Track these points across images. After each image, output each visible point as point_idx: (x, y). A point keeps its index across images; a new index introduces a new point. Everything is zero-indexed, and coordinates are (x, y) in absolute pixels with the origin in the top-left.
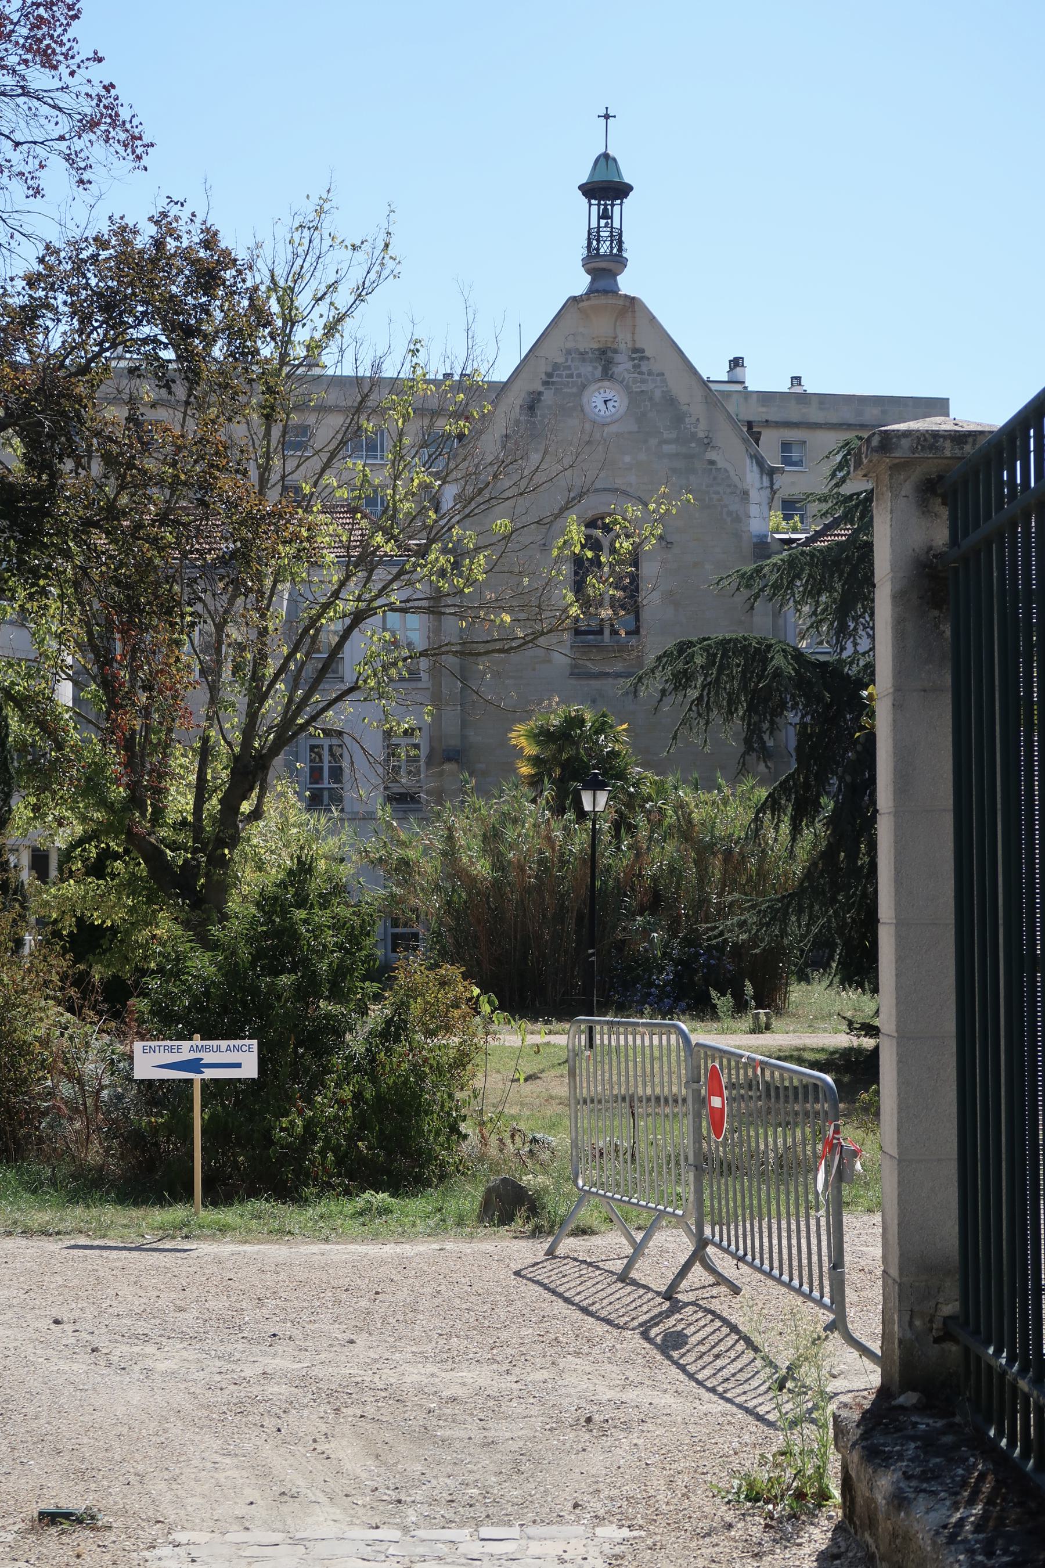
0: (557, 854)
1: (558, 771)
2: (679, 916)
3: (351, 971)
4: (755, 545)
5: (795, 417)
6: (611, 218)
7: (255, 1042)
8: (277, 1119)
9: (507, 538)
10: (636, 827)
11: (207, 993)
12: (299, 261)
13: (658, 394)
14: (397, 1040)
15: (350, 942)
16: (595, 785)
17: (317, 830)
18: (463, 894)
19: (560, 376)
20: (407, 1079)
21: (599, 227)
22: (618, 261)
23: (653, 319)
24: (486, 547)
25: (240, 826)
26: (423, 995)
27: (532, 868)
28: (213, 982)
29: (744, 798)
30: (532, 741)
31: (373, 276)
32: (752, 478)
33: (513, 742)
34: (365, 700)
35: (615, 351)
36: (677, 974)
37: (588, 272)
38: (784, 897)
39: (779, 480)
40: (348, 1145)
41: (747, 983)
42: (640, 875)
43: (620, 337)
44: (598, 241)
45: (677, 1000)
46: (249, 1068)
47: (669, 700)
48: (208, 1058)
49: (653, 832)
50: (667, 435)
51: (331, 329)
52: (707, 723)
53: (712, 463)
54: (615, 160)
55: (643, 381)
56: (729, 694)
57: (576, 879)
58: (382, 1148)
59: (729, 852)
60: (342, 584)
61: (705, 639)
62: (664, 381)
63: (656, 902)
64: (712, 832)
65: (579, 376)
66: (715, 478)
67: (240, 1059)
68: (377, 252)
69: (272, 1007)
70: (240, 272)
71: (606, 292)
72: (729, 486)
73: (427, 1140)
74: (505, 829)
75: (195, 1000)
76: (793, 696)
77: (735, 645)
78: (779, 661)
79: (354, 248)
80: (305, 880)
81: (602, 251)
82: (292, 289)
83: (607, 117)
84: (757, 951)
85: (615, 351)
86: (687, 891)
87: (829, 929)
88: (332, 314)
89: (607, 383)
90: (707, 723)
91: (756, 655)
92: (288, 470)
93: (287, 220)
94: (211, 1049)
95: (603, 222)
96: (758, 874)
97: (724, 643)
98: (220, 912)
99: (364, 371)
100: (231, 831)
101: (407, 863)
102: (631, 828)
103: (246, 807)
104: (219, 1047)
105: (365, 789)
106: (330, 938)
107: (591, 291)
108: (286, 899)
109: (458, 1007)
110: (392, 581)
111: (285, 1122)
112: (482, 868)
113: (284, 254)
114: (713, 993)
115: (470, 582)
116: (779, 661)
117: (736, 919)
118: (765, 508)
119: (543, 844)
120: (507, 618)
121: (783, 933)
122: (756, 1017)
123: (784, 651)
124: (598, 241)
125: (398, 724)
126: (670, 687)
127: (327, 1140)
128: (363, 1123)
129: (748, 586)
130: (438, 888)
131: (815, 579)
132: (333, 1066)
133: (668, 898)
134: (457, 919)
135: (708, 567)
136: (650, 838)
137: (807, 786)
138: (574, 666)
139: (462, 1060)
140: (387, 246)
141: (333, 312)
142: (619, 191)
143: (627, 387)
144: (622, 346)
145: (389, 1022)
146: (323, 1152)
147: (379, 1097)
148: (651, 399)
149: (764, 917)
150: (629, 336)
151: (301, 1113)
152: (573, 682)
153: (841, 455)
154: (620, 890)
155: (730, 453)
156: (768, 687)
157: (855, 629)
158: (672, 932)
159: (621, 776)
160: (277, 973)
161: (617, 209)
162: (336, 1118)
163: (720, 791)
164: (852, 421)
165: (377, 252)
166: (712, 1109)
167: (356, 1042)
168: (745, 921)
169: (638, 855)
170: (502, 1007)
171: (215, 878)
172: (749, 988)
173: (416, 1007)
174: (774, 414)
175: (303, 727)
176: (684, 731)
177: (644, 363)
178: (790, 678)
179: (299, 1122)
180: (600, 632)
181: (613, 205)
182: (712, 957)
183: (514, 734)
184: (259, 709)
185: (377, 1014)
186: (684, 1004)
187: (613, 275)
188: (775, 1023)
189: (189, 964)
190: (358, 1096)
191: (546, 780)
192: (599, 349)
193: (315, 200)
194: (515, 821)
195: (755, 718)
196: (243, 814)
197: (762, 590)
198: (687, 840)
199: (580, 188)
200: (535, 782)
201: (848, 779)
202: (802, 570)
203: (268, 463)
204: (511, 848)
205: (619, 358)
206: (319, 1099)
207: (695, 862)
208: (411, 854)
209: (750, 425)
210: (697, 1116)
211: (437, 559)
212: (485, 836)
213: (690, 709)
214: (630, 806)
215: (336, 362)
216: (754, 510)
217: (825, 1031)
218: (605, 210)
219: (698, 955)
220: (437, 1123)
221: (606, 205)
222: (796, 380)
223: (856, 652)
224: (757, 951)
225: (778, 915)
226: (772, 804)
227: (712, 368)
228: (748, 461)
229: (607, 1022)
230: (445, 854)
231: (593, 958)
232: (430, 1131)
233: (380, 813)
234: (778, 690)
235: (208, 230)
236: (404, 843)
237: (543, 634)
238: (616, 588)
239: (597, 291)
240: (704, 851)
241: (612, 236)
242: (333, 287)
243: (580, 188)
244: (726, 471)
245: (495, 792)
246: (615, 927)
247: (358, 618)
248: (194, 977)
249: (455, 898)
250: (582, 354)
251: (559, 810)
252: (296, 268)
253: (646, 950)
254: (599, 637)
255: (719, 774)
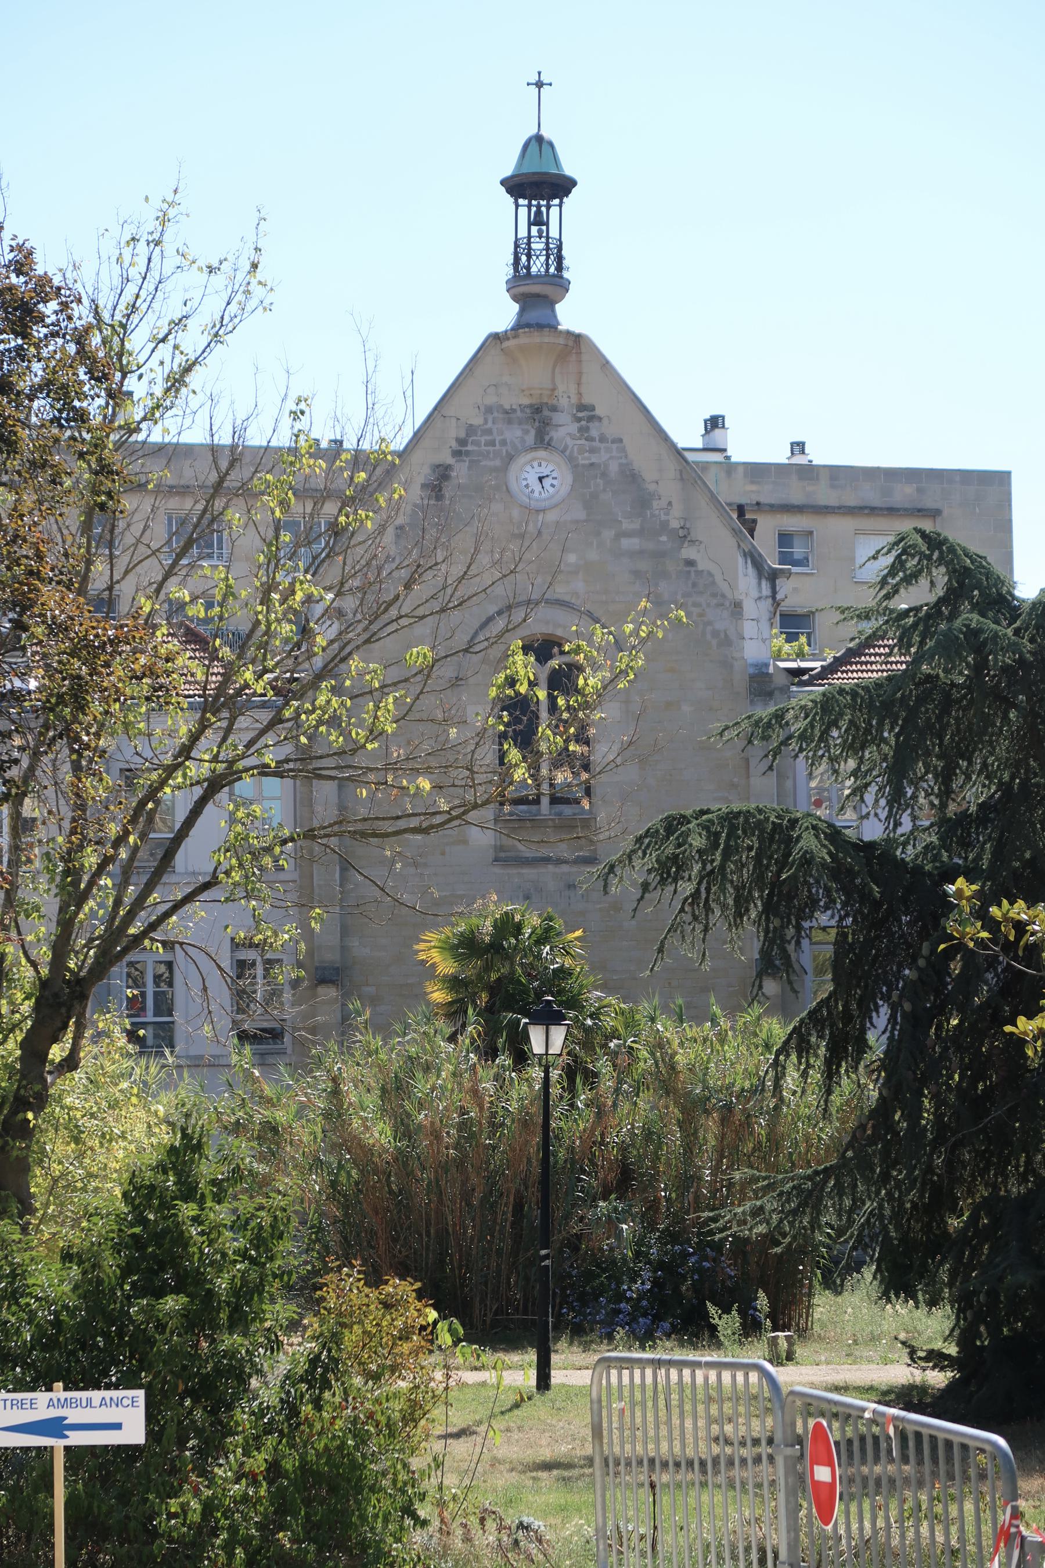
0: (486, 1114)
1: (485, 996)
2: (657, 1199)
3: (259, 1289)
4: (752, 677)
5: (796, 497)
6: (547, 224)
7: (141, 1393)
8: (162, 1501)
9: (427, 672)
10: (596, 1075)
11: (57, 1323)
12: (131, 290)
13: (614, 468)
14: (326, 1385)
15: (257, 1248)
16: (549, 1018)
17: (145, 1083)
18: (354, 1173)
19: (476, 443)
20: (343, 1444)
21: (529, 237)
22: (557, 283)
23: (605, 365)
24: (395, 684)
25: (49, 1079)
26: (361, 1322)
27: (451, 1135)
28: (66, 1307)
29: (749, 1033)
30: (447, 954)
31: (233, 308)
32: (747, 585)
33: (422, 956)
34: (227, 900)
35: (554, 409)
36: (655, 1283)
37: (515, 298)
38: (817, 1173)
39: (784, 587)
40: (264, 1539)
41: (761, 1294)
42: (602, 1143)
43: (561, 388)
44: (529, 256)
45: (657, 1318)
46: (133, 1431)
47: (652, 896)
48: (74, 1416)
49: (620, 1082)
50: (626, 525)
51: (176, 382)
52: (706, 930)
53: (690, 563)
54: (551, 144)
55: (592, 451)
56: (737, 889)
57: (513, 1150)
58: (311, 1540)
59: (729, 1108)
60: (194, 738)
61: (703, 812)
62: (623, 450)
63: (625, 1180)
64: (704, 1082)
65: (504, 443)
66: (694, 585)
67: (118, 1417)
68: (240, 276)
69: (151, 1342)
70: (65, 306)
71: (540, 326)
72: (714, 595)
73: (372, 1529)
74: (412, 1078)
75: (40, 1332)
76: (828, 890)
77: (746, 820)
78: (808, 842)
79: (211, 270)
80: (192, 1161)
81: (534, 270)
82: (124, 326)
83: (539, 85)
84: (778, 1250)
85: (554, 409)
86: (668, 1164)
87: (881, 1217)
88: (177, 361)
89: (542, 453)
90: (706, 930)
91: (777, 834)
92: (116, 577)
93: (115, 231)
94: (78, 1404)
95: (534, 230)
96: (768, 1140)
97: (730, 818)
98: (21, 1201)
99: (224, 438)
100: (37, 1087)
101: (274, 1130)
102: (591, 1077)
103: (57, 1052)
104: (89, 1401)
105: (204, 1019)
106: (233, 1243)
107: (520, 325)
108: (167, 1189)
109: (408, 1339)
110: (263, 732)
111: (174, 1505)
112: (380, 1135)
113: (110, 277)
114: (712, 1309)
115: (375, 733)
116: (808, 842)
117: (748, 1206)
118: (767, 625)
119: (468, 1102)
120: (425, 784)
121: (815, 1224)
122: (774, 1342)
123: (814, 827)
124: (529, 256)
125: (276, 934)
126: (654, 879)
127: (233, 1529)
128: (282, 1507)
129: (765, 738)
130: (317, 1164)
131: (858, 729)
132: (237, 1424)
133: (643, 1175)
134: (346, 1207)
135: (686, 708)
136: (617, 1091)
137: (847, 1017)
138: (499, 848)
139: (414, 1413)
140: (255, 266)
141: (179, 359)
142: (560, 187)
143: (571, 459)
144: (564, 402)
145: (314, 1361)
146: (228, 1547)
147: (304, 1466)
148: (604, 475)
149: (788, 1201)
150: (573, 389)
151: (196, 1492)
152: (498, 870)
153: (894, 553)
154: (574, 1166)
155: (716, 548)
156: (793, 877)
157: (914, 797)
158: (649, 1219)
159: (574, 1003)
160: (159, 1294)
161: (554, 211)
162: (245, 1498)
163: (714, 1020)
164: (877, 503)
165: (240, 276)
166: (816, 1484)
167: (266, 1390)
168: (761, 1208)
169: (600, 1115)
170: (470, 1339)
171: (15, 1153)
172: (762, 1301)
173: (351, 1338)
174: (767, 494)
175: (137, 939)
176: (674, 940)
177: (594, 426)
178: (824, 865)
179: (195, 1504)
180: (537, 801)
181: (548, 207)
182: (705, 1258)
183: (422, 946)
184: (77, 913)
185: (298, 1348)
186: (666, 1325)
187: (550, 303)
188: (799, 1351)
189: (30, 1281)
190: (274, 1469)
191: (470, 1011)
192: (531, 406)
193: (156, 203)
194: (427, 1068)
195: (776, 922)
196: (52, 1062)
197: (785, 742)
198: (668, 1094)
199: (503, 183)
200: (455, 1012)
201: (907, 1006)
202: (841, 714)
203: (88, 570)
204: (421, 1106)
205: (559, 418)
206: (219, 1472)
207: (680, 1124)
208: (281, 1116)
209: (741, 510)
210: (792, 1493)
211: (328, 702)
212: (384, 1090)
213: (682, 910)
214: (587, 1045)
215: (185, 426)
216: (749, 629)
217: (870, 1361)
218: (539, 213)
219: (686, 1255)
220: (386, 1504)
221: (539, 207)
222: (798, 447)
223: (915, 828)
224: (778, 1250)
225: (809, 1198)
226: (799, 1042)
227: (687, 435)
228: (740, 560)
229: (652, 1362)
230: (327, 1115)
231: (547, 1262)
232: (376, 1516)
233: (235, 1058)
234: (806, 882)
235: (20, 248)
236: (269, 1101)
237: (476, 806)
238: (577, 742)
239: (528, 325)
240: (692, 1109)
241: (547, 249)
242: (179, 323)
243: (503, 183)
244: (710, 574)
245: (398, 1027)
246: (567, 1217)
247: (214, 785)
248: (38, 1299)
249: (343, 1178)
250: (508, 414)
251: (490, 1053)
252: (128, 297)
253: (612, 1249)
254: (534, 808)
255: (713, 1000)
